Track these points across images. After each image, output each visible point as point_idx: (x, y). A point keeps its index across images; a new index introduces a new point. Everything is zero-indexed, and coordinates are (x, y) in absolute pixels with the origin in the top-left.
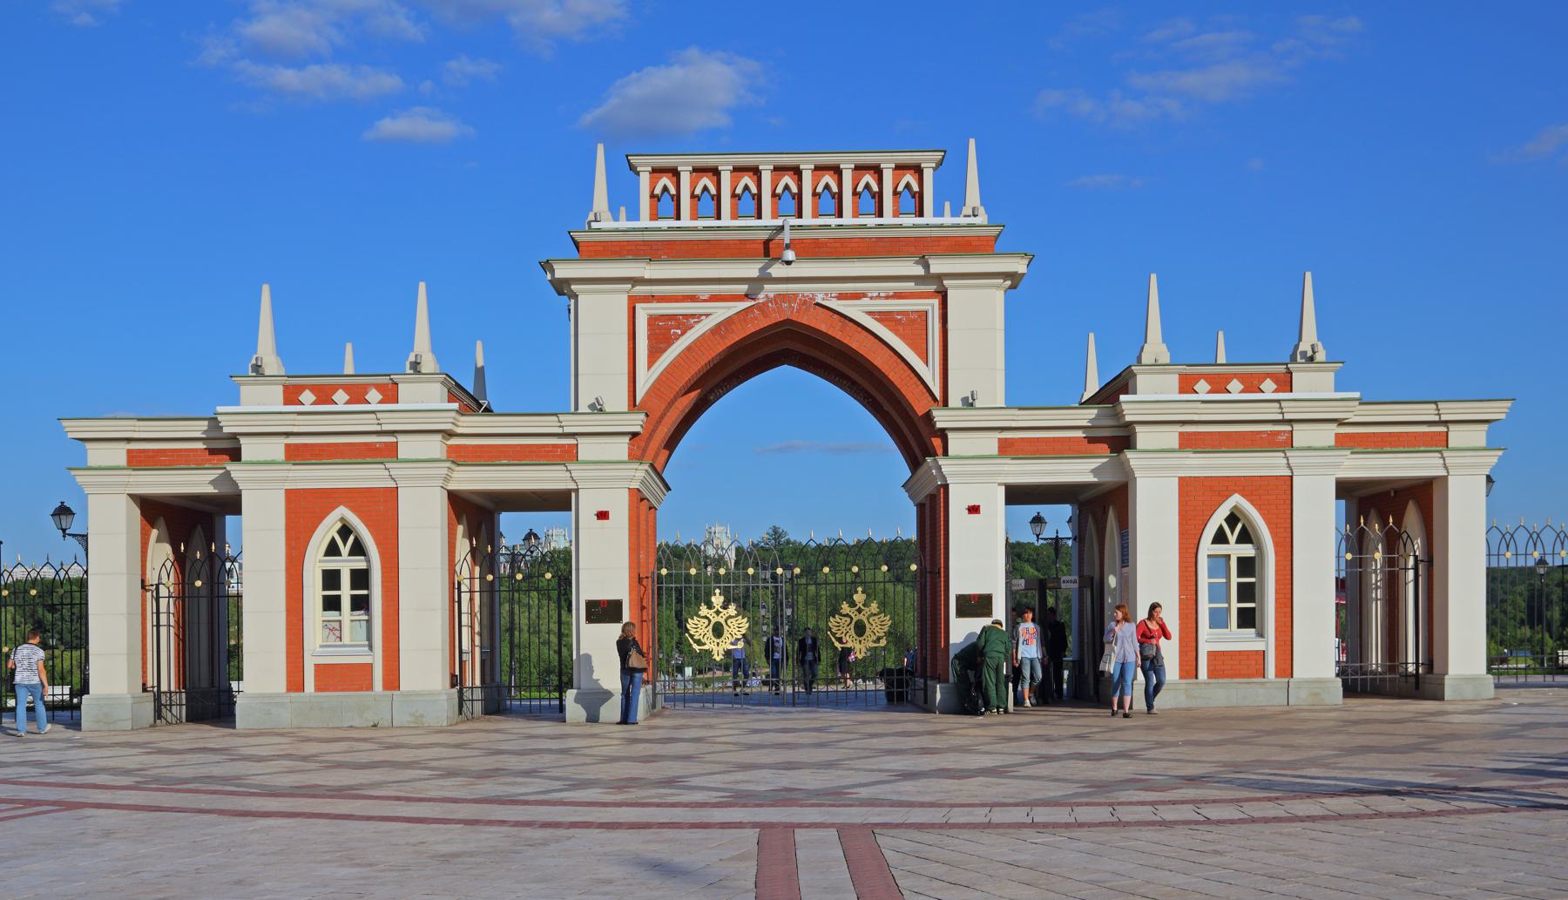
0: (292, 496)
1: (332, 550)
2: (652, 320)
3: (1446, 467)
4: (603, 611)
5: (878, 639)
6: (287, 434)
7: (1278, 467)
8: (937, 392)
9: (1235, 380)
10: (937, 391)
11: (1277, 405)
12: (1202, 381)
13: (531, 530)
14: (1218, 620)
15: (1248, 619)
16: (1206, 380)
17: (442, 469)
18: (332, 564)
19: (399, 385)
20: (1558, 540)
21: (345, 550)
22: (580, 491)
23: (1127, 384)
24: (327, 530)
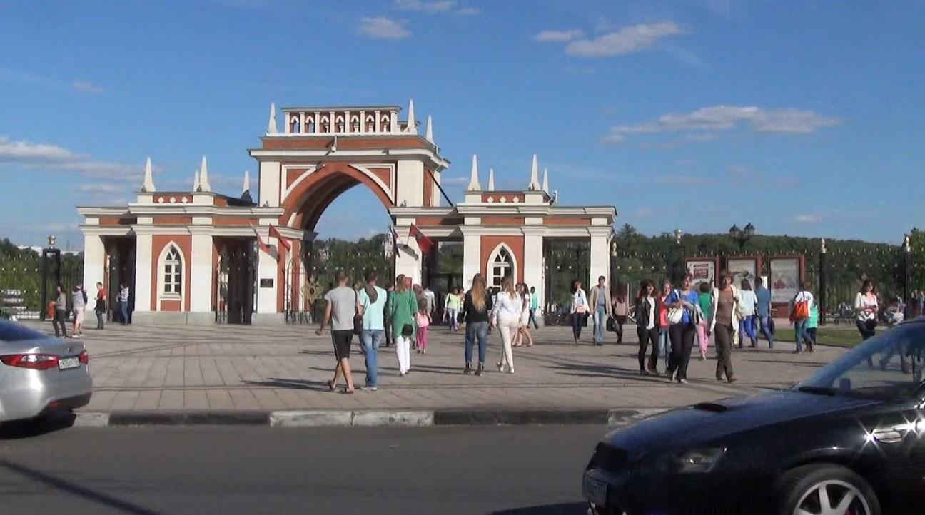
1: (498, 259)
3: (522, 232)
4: (267, 283)
7: (518, 232)
21: (503, 260)
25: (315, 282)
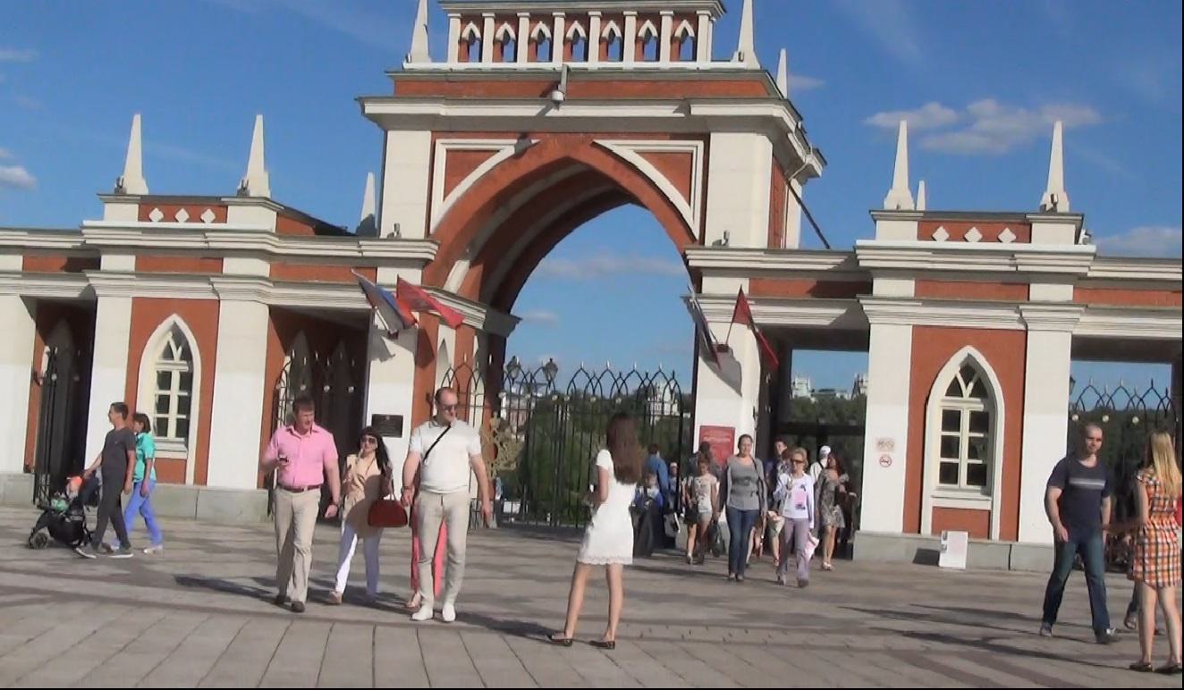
0: (138, 303)
1: (954, 390)
3: (1022, 320)
5: (508, 465)
8: (697, 234)
13: (551, 360)
14: (949, 474)
15: (979, 476)
18: (954, 403)
19: (1034, 225)
20: (668, 388)
21: (967, 390)
22: (221, 302)
24: (951, 370)
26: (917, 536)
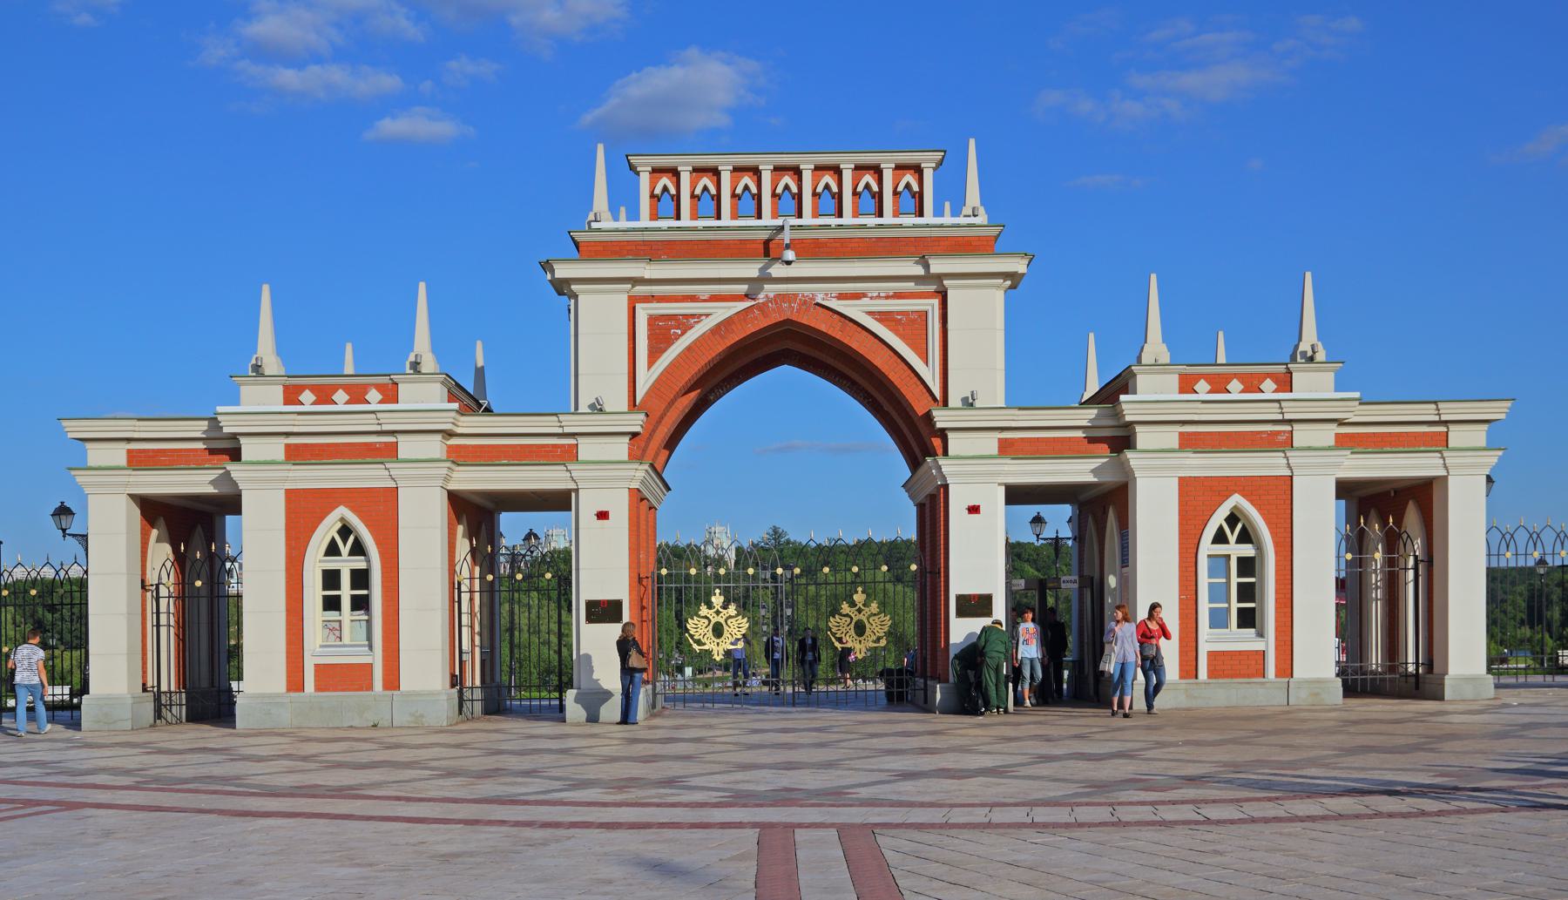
0: (292, 496)
1: (332, 550)
2: (652, 320)
3: (1446, 467)
4: (603, 611)
6: (287, 434)
7: (1278, 467)
8: (937, 392)
9: (1235, 380)
10: (937, 391)
11: (1277, 405)
12: (1202, 381)
14: (1218, 620)
15: (1248, 619)
16: (1206, 380)
17: (442, 469)
18: (332, 564)
19: (399, 385)
21: (345, 550)
22: (580, 491)
23: (1127, 384)
24: (327, 530)
25: (725, 607)
26: (1193, 681)
